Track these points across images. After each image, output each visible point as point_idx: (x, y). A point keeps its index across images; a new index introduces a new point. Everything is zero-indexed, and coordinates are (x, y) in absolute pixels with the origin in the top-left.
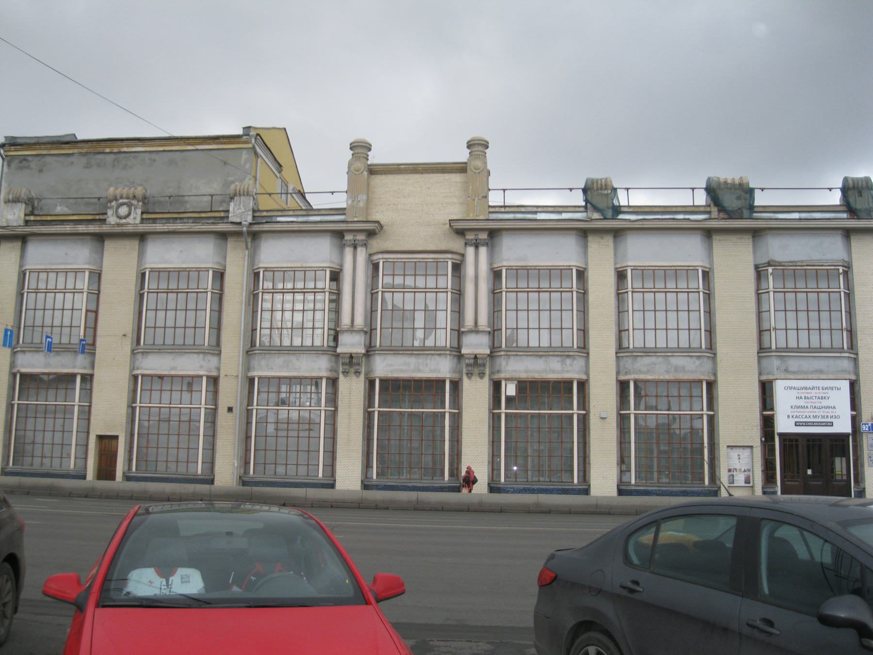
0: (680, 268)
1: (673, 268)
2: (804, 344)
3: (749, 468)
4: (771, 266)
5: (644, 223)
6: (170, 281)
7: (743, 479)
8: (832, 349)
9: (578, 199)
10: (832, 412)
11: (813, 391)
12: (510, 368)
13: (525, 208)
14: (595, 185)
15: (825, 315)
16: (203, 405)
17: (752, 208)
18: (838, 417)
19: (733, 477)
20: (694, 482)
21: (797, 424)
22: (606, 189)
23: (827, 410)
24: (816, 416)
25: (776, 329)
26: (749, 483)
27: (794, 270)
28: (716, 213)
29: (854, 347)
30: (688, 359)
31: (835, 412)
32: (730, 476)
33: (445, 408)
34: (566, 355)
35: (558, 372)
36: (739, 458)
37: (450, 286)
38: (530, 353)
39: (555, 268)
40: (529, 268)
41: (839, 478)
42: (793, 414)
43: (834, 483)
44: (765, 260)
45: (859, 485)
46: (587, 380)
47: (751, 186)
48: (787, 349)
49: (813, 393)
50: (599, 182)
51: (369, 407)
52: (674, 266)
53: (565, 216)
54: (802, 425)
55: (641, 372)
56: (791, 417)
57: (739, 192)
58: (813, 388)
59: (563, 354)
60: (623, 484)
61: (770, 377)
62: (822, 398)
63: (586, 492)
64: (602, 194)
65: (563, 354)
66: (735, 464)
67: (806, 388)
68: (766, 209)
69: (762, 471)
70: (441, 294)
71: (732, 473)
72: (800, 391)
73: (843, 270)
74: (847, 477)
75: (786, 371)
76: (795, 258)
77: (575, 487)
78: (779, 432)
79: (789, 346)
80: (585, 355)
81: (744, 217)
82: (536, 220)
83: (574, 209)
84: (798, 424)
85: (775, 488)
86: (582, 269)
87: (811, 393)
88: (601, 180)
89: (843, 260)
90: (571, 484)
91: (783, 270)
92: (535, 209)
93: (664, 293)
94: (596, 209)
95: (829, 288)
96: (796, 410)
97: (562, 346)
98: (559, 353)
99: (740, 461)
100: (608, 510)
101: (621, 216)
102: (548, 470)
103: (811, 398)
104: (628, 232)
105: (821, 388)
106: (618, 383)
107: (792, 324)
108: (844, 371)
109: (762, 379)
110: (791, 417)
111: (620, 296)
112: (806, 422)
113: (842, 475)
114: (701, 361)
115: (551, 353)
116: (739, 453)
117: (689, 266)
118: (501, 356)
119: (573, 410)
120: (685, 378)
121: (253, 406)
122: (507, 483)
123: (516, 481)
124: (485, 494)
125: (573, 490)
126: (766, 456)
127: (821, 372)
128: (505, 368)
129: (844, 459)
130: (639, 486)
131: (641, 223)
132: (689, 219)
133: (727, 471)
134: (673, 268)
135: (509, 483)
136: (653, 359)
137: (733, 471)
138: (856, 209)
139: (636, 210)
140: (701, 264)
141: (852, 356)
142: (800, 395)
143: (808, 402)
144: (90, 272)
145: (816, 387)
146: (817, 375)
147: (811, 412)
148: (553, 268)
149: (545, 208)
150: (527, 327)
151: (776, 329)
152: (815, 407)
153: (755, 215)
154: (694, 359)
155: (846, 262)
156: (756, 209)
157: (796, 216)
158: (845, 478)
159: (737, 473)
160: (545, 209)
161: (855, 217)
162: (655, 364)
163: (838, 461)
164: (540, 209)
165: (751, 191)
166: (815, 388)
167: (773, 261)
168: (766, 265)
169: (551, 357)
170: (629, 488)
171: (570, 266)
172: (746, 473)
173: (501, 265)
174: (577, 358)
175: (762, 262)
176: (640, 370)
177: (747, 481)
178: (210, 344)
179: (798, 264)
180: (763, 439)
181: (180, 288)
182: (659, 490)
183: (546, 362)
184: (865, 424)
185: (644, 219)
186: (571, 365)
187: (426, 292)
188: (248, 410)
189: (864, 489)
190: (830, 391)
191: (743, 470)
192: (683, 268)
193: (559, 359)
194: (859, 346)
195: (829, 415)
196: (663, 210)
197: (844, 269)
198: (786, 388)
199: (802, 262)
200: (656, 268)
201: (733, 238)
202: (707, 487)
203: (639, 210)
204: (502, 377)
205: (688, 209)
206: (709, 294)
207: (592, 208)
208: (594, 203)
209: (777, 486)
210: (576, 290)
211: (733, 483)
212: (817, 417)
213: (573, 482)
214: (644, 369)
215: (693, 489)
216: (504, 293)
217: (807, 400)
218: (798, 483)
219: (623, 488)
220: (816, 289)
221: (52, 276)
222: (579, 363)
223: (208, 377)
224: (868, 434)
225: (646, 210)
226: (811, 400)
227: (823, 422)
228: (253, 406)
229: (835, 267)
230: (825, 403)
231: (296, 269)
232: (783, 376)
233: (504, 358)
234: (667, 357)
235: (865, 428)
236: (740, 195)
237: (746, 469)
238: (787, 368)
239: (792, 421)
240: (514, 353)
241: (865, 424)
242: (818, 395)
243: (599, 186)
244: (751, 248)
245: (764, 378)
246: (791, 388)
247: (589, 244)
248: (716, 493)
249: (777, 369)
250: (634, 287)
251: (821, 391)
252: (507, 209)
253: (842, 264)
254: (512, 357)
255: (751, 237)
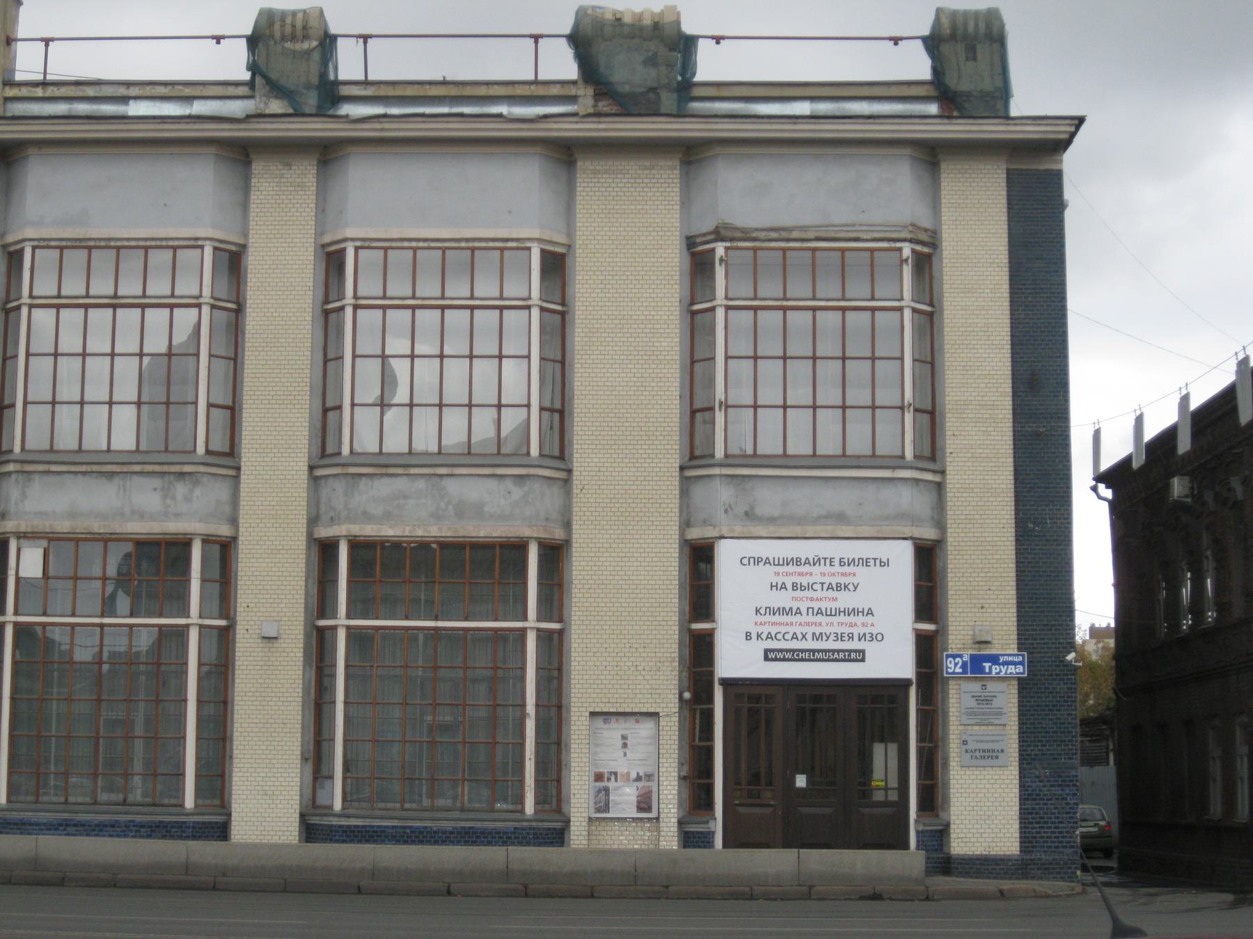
0: (483, 244)
1: (463, 244)
2: (799, 445)
3: (650, 770)
4: (722, 240)
5: (387, 126)
6: (876, 277)
7: (634, 799)
8: (873, 460)
9: (918, 66)
10: (863, 624)
11: (816, 570)
12: (30, 506)
13: (97, 88)
14: (277, 27)
15: (858, 370)
16: (194, 617)
17: (686, 88)
18: (879, 637)
19: (607, 794)
20: (407, 806)
21: (768, 656)
22: (306, 37)
23: (852, 619)
24: (821, 634)
25: (727, 407)
26: (649, 809)
27: (784, 250)
28: (590, 102)
29: (938, 454)
30: (492, 484)
31: (872, 625)
32: (599, 791)
33: (525, 619)
34: (175, 473)
35: (153, 518)
36: (625, 745)
37: (207, 292)
38: (83, 468)
39: (158, 243)
40: (92, 243)
41: (878, 796)
42: (760, 629)
43: (866, 811)
44: (708, 225)
45: (937, 816)
46: (235, 539)
47: (688, 28)
48: (755, 459)
49: (817, 574)
50: (289, 20)
51: (322, 614)
52: (467, 240)
53: (199, 108)
54: (784, 660)
55: (367, 517)
56: (754, 636)
57: (652, 46)
58: (817, 561)
59: (166, 468)
60: (318, 811)
61: (709, 533)
62: (839, 587)
63: (222, 831)
64: (294, 54)
65: (166, 468)
66: (614, 760)
67: (798, 562)
68: (723, 90)
69: (682, 778)
70: (513, 312)
71: (605, 784)
72: (781, 569)
73: (913, 251)
74: (900, 797)
75: (750, 515)
76: (787, 221)
77: (183, 819)
78: (720, 676)
79: (790, 452)
80: (232, 472)
81: (663, 110)
82: (124, 118)
83: (222, 89)
84: (771, 655)
85: (708, 822)
86: (233, 248)
87: (811, 574)
88: (294, 13)
89: (913, 225)
90: (518, 816)
91: (755, 250)
92: (122, 91)
93: (439, 311)
94: (276, 89)
95: (873, 299)
96: (768, 618)
97: (814, 455)
98: (157, 468)
99: (627, 751)
100: (747, 889)
101: (348, 109)
102: (426, 780)
103: (810, 587)
104: (718, 150)
105: (837, 562)
106: (315, 549)
107: (772, 394)
108: (901, 516)
109: (695, 536)
110: (754, 636)
111: (329, 317)
112: (793, 651)
113: (886, 789)
114: (526, 488)
115: (137, 468)
116: (625, 732)
117: (507, 240)
118: (9, 473)
119: (188, 617)
120: (481, 535)
121: (334, 617)
122: (13, 806)
123: (66, 802)
124: (290, 846)
125: (181, 826)
126: (694, 741)
127: (841, 518)
128: (16, 504)
129: (893, 748)
130: (349, 817)
131: (378, 126)
132: (500, 115)
133: (592, 778)
134: (463, 244)
135: (19, 806)
136: (400, 484)
137: (609, 779)
138: (956, 92)
139: (383, 91)
140: (536, 234)
141: (929, 477)
142: (780, 580)
143: (801, 599)
144: (215, 249)
145: (825, 559)
146: (829, 528)
147: (808, 624)
148: (153, 243)
149: (148, 88)
150: (781, 403)
151: (727, 407)
152: (820, 612)
153: (697, 106)
154: (509, 484)
155: (926, 230)
156: (697, 92)
157: (803, 108)
158: (893, 796)
159: (619, 783)
160: (148, 91)
161: (955, 114)
162: (405, 497)
163: (878, 750)
164: (134, 91)
165: (687, 45)
166: (822, 561)
167: (728, 227)
168: (712, 237)
169: (136, 479)
170: (327, 821)
171: (197, 239)
172: (640, 784)
173: (20, 237)
174: (205, 479)
175: (704, 230)
176: (365, 513)
177: (643, 805)
178: (211, 448)
179: (795, 235)
180: (687, 695)
181: (447, 294)
182: (404, 827)
183: (125, 490)
184: (954, 657)
185: (385, 116)
186: (188, 499)
187: (384, 308)
188: (321, 631)
189: (947, 825)
190: (860, 570)
191: (633, 775)
192: (491, 244)
193: (157, 482)
194: (948, 451)
195: (856, 631)
196: (454, 91)
197: (919, 248)
198: (745, 561)
199: (803, 228)
200: (421, 244)
201: (631, 167)
202: (193, 814)
203: (391, 92)
204: (8, 530)
205: (519, 91)
206: (931, 315)
207: (267, 88)
208: (273, 76)
209: (715, 819)
210: (540, 303)
211: (606, 808)
212: (825, 638)
213: (522, 811)
214: (377, 510)
215: (499, 825)
216: (720, 313)
217: (798, 593)
218: (767, 811)
219: (315, 820)
220: (838, 300)
221: (103, 260)
222: (212, 494)
223: (207, 541)
224: (961, 682)
225: (410, 91)
226: (810, 594)
227: (839, 651)
228: (334, 617)
229: (893, 245)
230: (846, 600)
231: (477, 244)
232: (738, 530)
233: (17, 481)
234: (436, 478)
235: (952, 665)
236: (656, 54)
237: (641, 774)
238: (752, 508)
239: (759, 647)
240: (41, 468)
241: (954, 657)
242: (827, 580)
243: (288, 30)
244: (675, 193)
245: (694, 534)
246: (758, 561)
247: (254, 180)
248: (558, 836)
249: (726, 511)
250: (35, 293)
251: (837, 568)
252: (51, 92)
253: (909, 236)
254: (36, 477)
255: (677, 163)
